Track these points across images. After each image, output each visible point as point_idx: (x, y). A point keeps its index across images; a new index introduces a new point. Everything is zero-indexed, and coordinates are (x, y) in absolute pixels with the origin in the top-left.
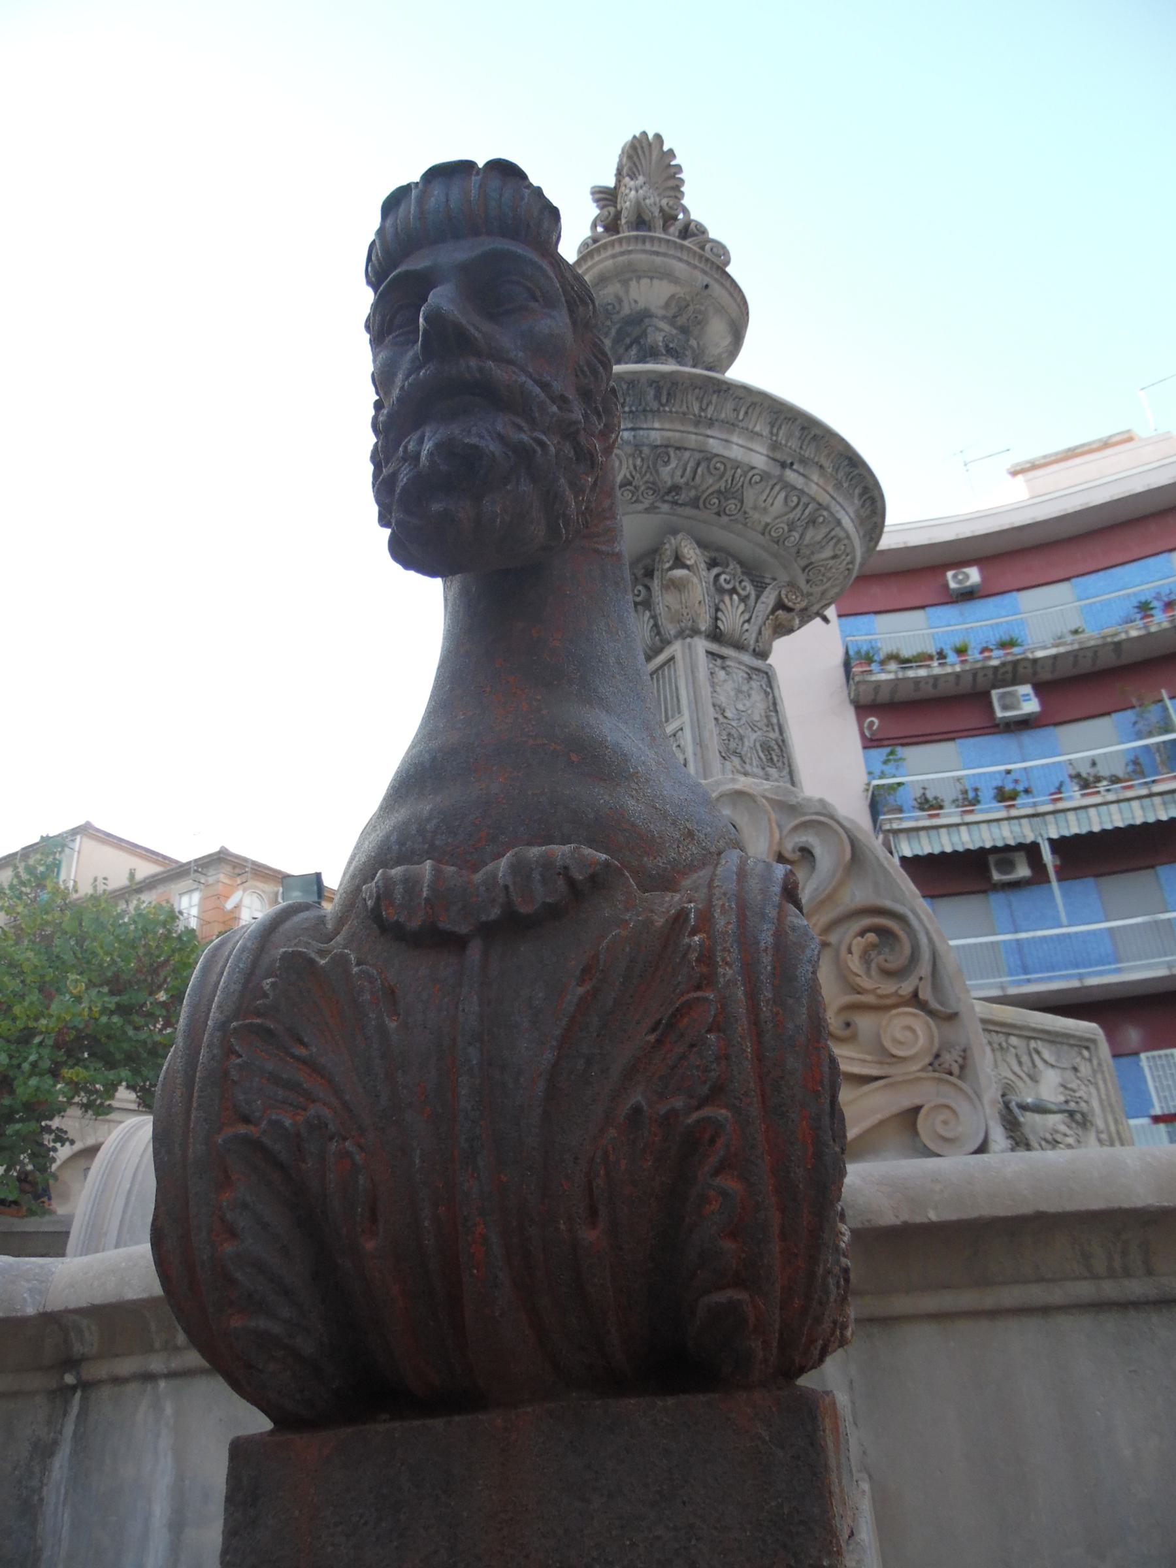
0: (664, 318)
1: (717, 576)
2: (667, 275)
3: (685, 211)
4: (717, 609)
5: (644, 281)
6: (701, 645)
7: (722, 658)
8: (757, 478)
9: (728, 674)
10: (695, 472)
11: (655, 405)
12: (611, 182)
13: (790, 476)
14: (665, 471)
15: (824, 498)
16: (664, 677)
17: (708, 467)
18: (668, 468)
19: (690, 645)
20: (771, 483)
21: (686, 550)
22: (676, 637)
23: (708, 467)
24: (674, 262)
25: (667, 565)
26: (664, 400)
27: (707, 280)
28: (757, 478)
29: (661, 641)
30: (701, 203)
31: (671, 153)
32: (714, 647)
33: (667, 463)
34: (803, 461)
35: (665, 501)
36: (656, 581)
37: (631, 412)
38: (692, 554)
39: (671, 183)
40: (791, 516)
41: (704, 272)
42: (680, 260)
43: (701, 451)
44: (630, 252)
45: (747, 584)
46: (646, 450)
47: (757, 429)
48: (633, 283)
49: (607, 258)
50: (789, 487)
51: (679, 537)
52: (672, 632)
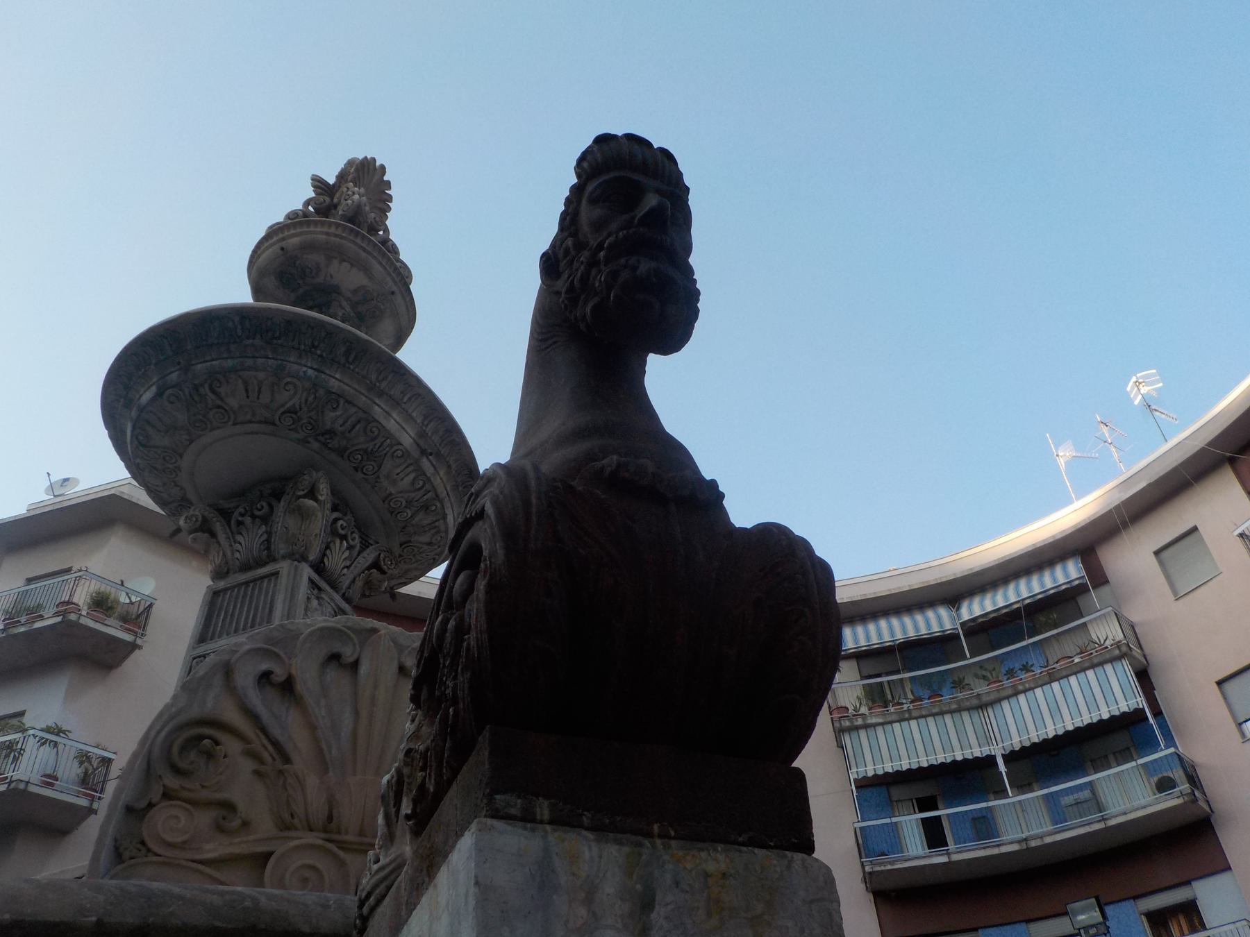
0: (348, 300)
1: (336, 520)
2: (366, 270)
3: (386, 230)
4: (328, 547)
5: (346, 265)
6: (307, 572)
7: (320, 589)
8: (399, 453)
9: (320, 604)
10: (354, 427)
11: (343, 360)
12: (331, 180)
13: (425, 463)
14: (330, 415)
15: (442, 492)
16: (260, 589)
17: (365, 428)
18: (333, 414)
19: (296, 568)
20: (409, 462)
21: (321, 487)
22: (284, 557)
23: (365, 428)
24: (374, 262)
25: (301, 493)
26: (351, 359)
27: (394, 288)
28: (399, 453)
29: (268, 556)
30: (401, 227)
31: (388, 183)
32: (316, 577)
33: (335, 409)
34: (438, 455)
35: (317, 440)
36: (282, 503)
37: (321, 356)
38: (324, 491)
39: (381, 205)
40: (413, 495)
41: (395, 283)
42: (380, 263)
43: (365, 412)
44: (342, 237)
45: (356, 535)
46: (321, 392)
47: (414, 415)
48: (335, 263)
49: (322, 233)
50: (421, 472)
51: (320, 474)
52: (282, 552)
